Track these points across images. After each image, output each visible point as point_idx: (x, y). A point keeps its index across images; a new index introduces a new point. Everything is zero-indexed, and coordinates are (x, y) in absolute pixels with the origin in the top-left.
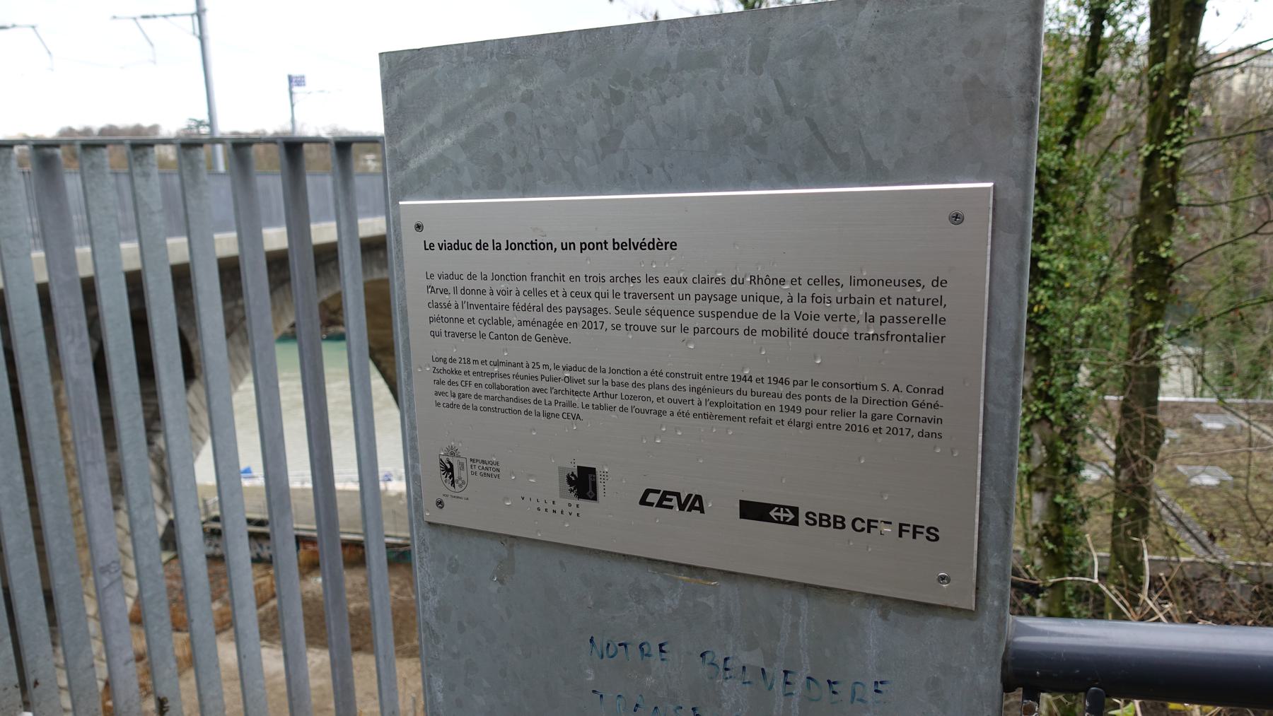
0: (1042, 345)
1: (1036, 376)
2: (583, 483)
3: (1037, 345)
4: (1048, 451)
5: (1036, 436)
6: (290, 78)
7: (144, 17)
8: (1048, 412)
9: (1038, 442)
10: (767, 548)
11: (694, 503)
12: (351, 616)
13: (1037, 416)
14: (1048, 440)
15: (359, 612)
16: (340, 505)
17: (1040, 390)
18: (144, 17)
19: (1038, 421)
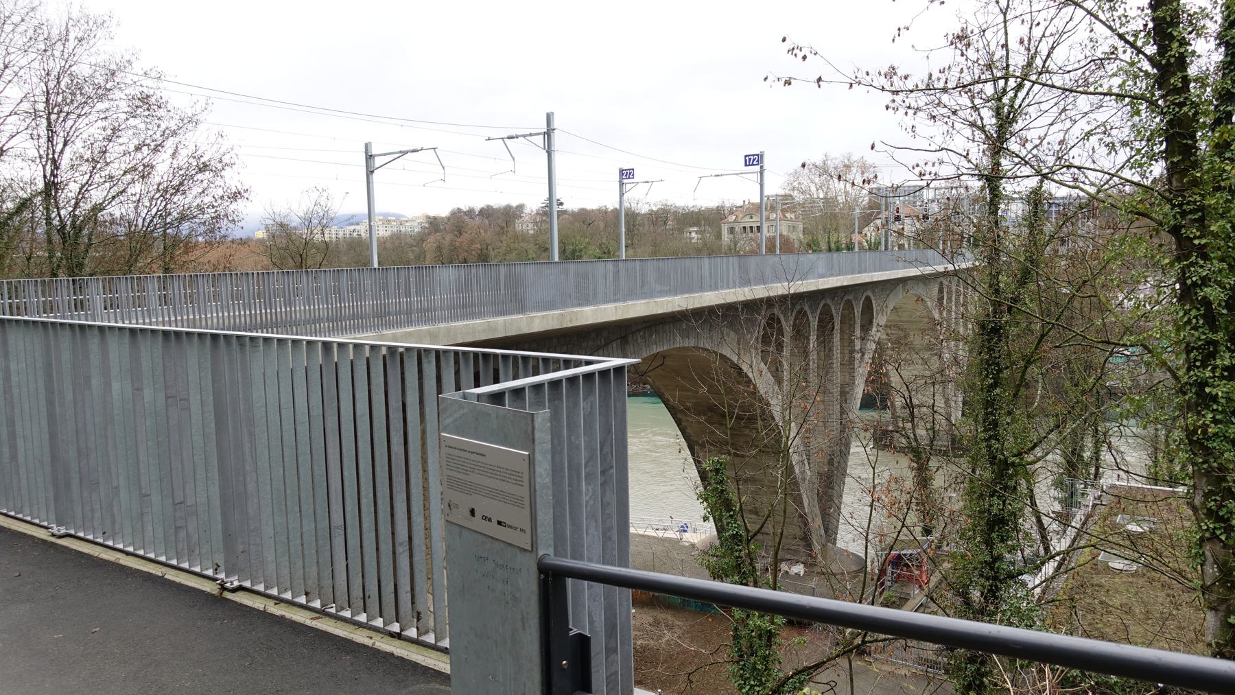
0: (1210, 466)
1: (1207, 496)
2: (472, 512)
3: (1205, 466)
4: (1220, 570)
5: (1208, 553)
6: (621, 171)
7: (510, 138)
8: (1218, 532)
9: (1210, 560)
10: (501, 533)
11: (490, 520)
12: (636, 651)
13: (1207, 535)
14: (1221, 558)
15: (645, 648)
16: (632, 549)
17: (1210, 510)
18: (510, 138)
19: (1208, 539)
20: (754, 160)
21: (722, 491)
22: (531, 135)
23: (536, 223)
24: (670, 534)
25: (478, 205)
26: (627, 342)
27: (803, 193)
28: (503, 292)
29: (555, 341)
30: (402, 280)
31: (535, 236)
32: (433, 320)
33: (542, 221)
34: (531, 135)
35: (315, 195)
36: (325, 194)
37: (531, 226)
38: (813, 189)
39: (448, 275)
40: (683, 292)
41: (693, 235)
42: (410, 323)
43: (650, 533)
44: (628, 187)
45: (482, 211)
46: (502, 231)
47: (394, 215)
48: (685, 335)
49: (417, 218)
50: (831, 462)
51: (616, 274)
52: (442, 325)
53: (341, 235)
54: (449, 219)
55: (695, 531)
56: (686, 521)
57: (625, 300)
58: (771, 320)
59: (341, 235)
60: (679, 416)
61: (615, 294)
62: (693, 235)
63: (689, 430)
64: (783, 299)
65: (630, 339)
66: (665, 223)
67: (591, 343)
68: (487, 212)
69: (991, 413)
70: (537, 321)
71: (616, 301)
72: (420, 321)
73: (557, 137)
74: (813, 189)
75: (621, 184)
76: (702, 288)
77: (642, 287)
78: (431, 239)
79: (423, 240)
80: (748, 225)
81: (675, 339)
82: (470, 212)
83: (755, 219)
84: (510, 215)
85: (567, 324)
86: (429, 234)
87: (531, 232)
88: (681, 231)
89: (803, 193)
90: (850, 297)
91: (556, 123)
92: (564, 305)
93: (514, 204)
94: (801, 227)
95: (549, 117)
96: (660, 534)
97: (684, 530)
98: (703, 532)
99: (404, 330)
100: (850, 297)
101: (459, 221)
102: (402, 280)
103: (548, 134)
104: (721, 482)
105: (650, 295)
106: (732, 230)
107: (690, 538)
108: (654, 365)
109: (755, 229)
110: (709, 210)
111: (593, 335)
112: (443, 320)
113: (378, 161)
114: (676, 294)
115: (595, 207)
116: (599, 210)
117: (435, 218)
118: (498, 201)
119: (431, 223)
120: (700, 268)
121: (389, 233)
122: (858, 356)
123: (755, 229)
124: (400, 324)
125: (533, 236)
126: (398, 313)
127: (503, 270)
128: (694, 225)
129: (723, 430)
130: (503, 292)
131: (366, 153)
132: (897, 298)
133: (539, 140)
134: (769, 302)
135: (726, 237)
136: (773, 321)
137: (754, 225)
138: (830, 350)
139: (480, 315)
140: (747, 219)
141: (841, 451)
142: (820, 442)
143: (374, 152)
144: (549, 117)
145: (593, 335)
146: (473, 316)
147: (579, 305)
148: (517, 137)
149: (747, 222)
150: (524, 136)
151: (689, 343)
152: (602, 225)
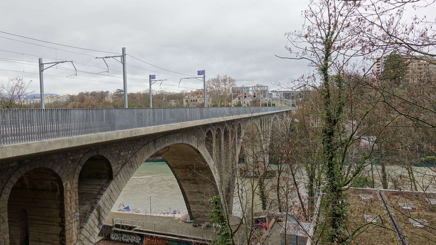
6: (150, 76)
7: (106, 57)
18: (106, 57)
20: (201, 73)
21: (219, 212)
22: (115, 57)
23: (113, 98)
24: (170, 215)
25: (90, 91)
26: (156, 142)
27: (211, 88)
28: (105, 121)
29: (126, 142)
30: (54, 116)
31: (113, 103)
32: (71, 134)
33: (116, 98)
34: (115, 57)
35: (16, 82)
36: (21, 81)
37: (111, 99)
38: (214, 87)
39: (78, 113)
40: (180, 121)
41: (173, 103)
42: (58, 136)
43: (162, 215)
44: (153, 82)
45: (92, 93)
46: (100, 101)
47: (55, 95)
48: (178, 139)
49: (65, 96)
50: (229, 184)
51: (154, 114)
52: (75, 137)
53: (32, 102)
54: (78, 96)
55: (179, 213)
56: (175, 209)
57: (158, 125)
58: (207, 132)
59: (32, 102)
60: (174, 170)
61: (153, 122)
62: (173, 103)
63: (178, 175)
64: (227, 121)
65: (157, 141)
66: (162, 99)
67: (141, 143)
68: (94, 94)
69: (332, 169)
70: (121, 134)
71: (154, 125)
72: (63, 135)
73: (127, 58)
74: (214, 87)
75: (150, 81)
76: (187, 120)
77: (164, 119)
78: (71, 104)
79: (67, 104)
80: (192, 99)
81: (174, 141)
82: (87, 94)
83: (195, 97)
84: (103, 95)
85: (134, 135)
86: (70, 102)
87: (111, 101)
88: (168, 101)
89: (211, 88)
90: (240, 122)
91: (126, 52)
92: (132, 127)
93: (105, 91)
94: (211, 100)
95: (124, 50)
96: (166, 215)
97: (175, 212)
98: (182, 213)
99: (55, 139)
100: (240, 122)
101: (82, 97)
102: (54, 116)
103: (123, 56)
104: (219, 208)
105: (167, 122)
106: (187, 101)
107: (177, 216)
108: (165, 150)
109: (195, 101)
110: (177, 94)
111: (142, 140)
112: (75, 134)
113: (45, 66)
114: (177, 122)
115: (136, 93)
116: (138, 94)
117: (72, 96)
118: (98, 89)
119: (71, 98)
120: (186, 111)
121: (53, 101)
122: (237, 144)
123: (195, 101)
124: (53, 136)
125: (112, 103)
126: (52, 131)
127: (105, 111)
128: (173, 99)
129: (190, 172)
130: (105, 121)
131: (40, 62)
132: (249, 123)
133: (119, 59)
134: (207, 126)
135: (185, 104)
136: (209, 133)
137: (195, 99)
138: (228, 143)
139: (94, 132)
140: (192, 97)
141: (233, 180)
142: (226, 176)
143: (43, 63)
144: (124, 50)
145: (142, 140)
146: (91, 132)
147: (139, 127)
148: (109, 57)
149: (192, 98)
150: (113, 57)
151: (180, 142)
152: (139, 99)
